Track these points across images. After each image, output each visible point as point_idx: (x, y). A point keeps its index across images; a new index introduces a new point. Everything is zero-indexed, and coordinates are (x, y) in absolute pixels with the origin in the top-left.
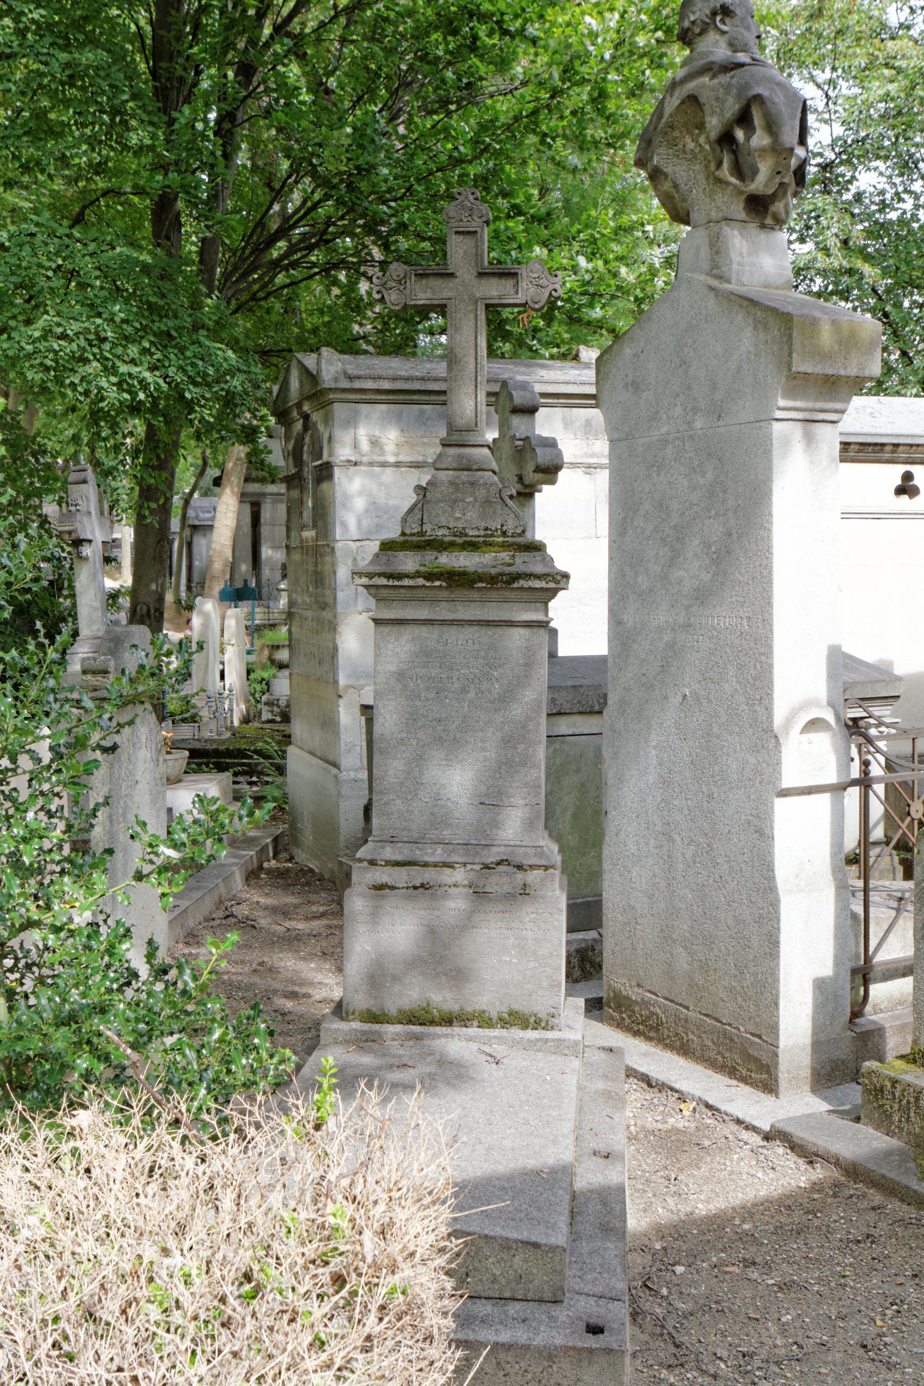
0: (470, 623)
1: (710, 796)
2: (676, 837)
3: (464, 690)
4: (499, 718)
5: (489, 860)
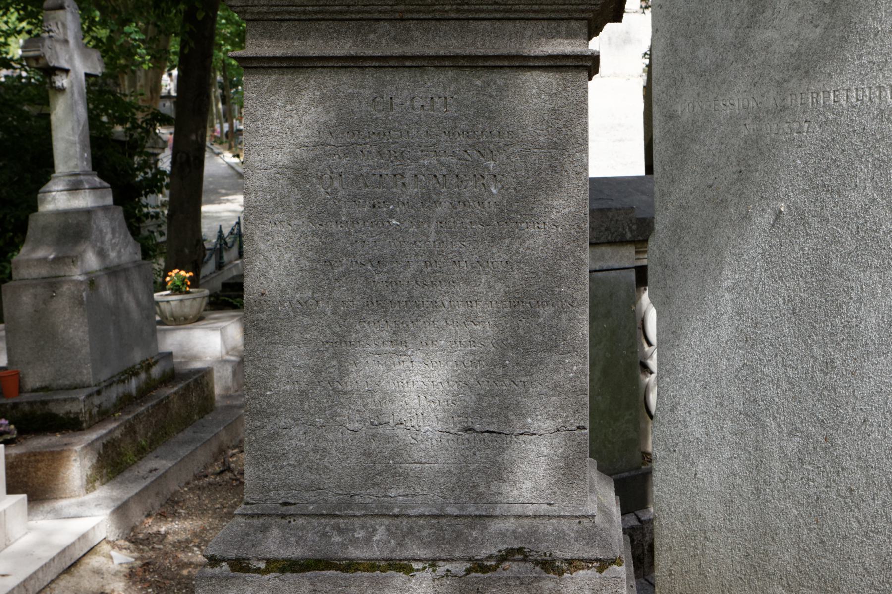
0: (439, 62)
1: (828, 365)
2: (768, 421)
3: (428, 200)
4: (499, 255)
5: (484, 553)
